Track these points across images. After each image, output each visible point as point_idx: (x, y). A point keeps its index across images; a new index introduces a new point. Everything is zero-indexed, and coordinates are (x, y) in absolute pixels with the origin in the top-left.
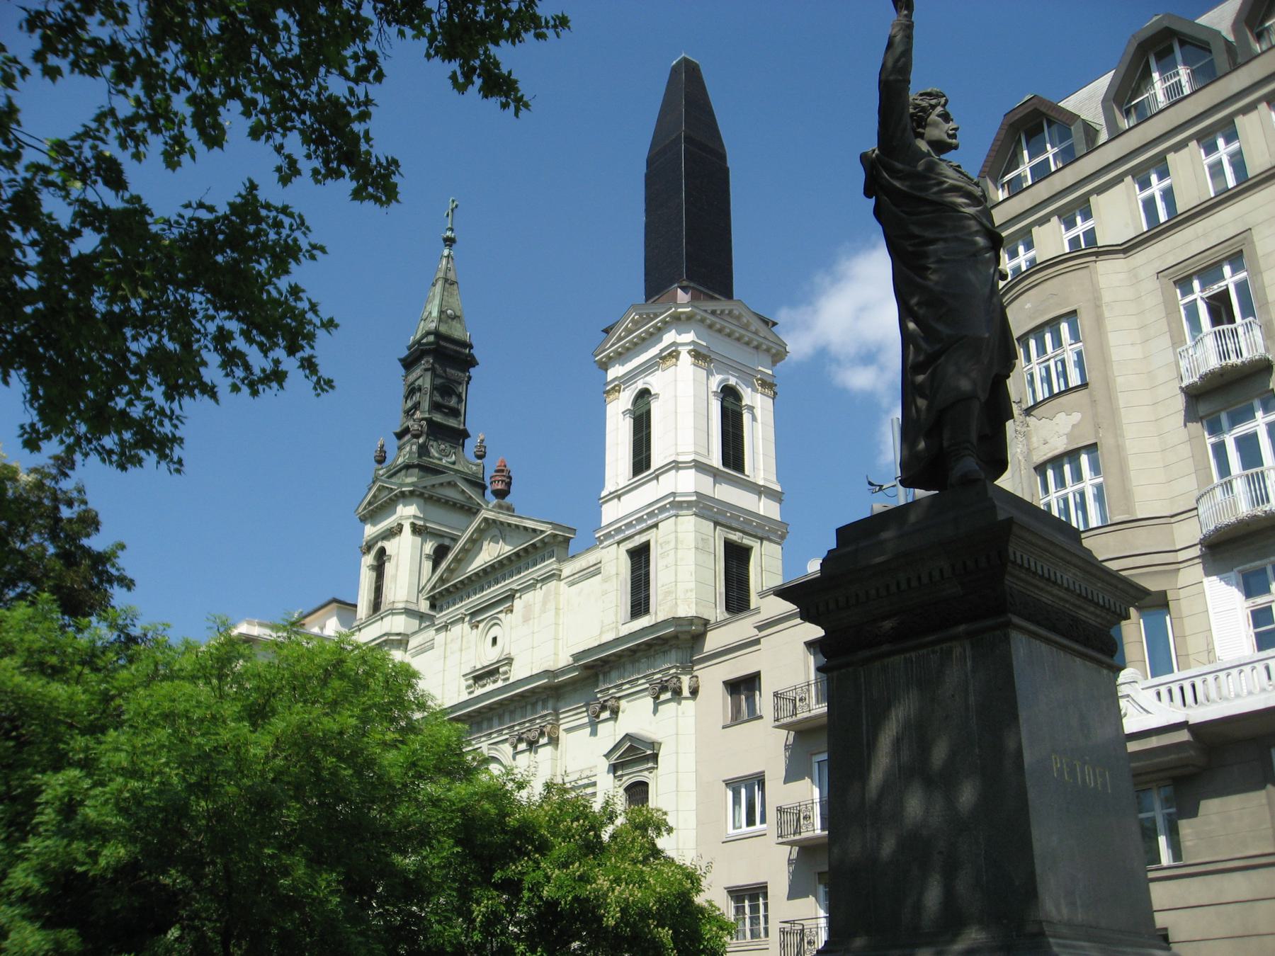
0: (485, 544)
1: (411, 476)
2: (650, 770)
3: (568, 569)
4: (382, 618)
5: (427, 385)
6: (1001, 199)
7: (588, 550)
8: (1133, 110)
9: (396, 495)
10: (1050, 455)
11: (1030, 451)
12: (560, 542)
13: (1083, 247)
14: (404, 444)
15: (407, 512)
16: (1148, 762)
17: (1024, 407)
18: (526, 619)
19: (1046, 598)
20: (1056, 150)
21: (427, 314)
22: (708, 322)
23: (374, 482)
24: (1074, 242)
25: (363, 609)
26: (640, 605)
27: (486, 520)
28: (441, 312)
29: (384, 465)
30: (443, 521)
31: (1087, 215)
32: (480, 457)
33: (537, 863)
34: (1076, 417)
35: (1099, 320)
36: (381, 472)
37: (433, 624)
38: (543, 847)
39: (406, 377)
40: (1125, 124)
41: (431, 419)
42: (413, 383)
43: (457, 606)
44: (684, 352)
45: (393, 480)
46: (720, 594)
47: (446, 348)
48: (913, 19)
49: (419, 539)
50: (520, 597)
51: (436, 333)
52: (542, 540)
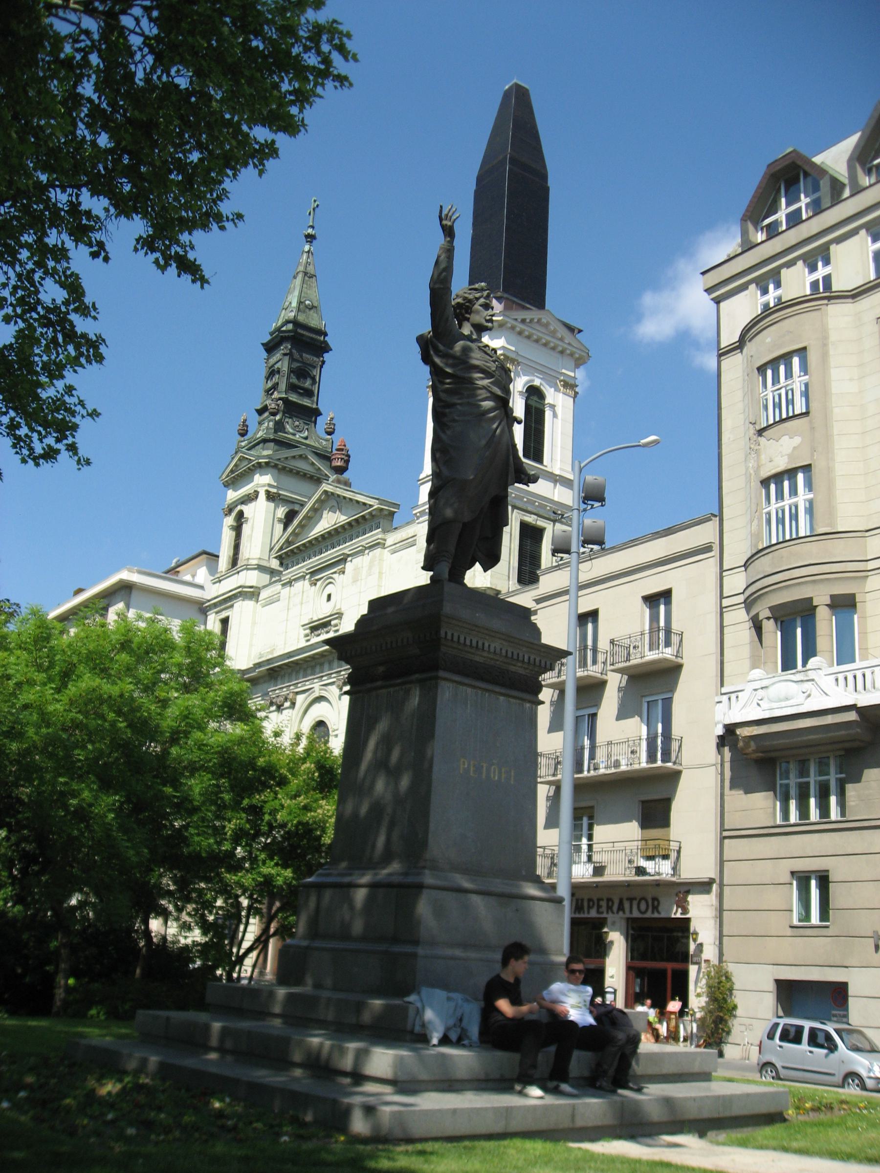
0: (325, 512)
1: (267, 449)
3: (392, 538)
4: (238, 572)
6: (759, 241)
7: (408, 523)
8: (874, 170)
9: (253, 465)
10: (774, 472)
11: (759, 467)
12: (386, 515)
13: (821, 290)
14: (264, 420)
15: (263, 481)
16: (824, 735)
17: (758, 428)
18: (355, 580)
19: (477, 659)
20: (808, 200)
21: (287, 303)
22: (518, 329)
23: (236, 453)
24: (815, 285)
25: (223, 563)
27: (326, 492)
28: (300, 303)
29: (246, 437)
30: (293, 489)
31: (827, 262)
32: (330, 433)
33: (276, 793)
34: (797, 440)
36: (243, 444)
37: (280, 580)
38: (283, 782)
39: (268, 359)
40: (865, 181)
41: (287, 398)
42: (273, 366)
43: (300, 565)
45: (251, 452)
46: (513, 568)
47: (303, 335)
48: (454, 244)
49: (272, 505)
50: (351, 561)
51: (295, 322)
52: (370, 513)
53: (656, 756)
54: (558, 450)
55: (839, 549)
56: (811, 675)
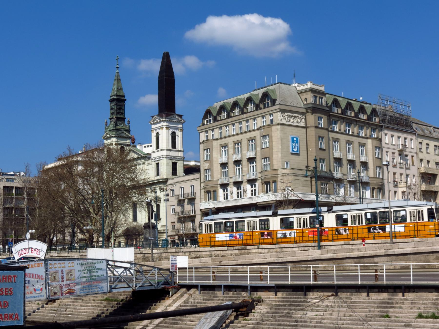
2: (160, 203)
3: (146, 162)
5: (116, 108)
26: (158, 174)
28: (117, 89)
32: (129, 124)
35: (212, 150)
44: (164, 127)
53: (377, 220)
54: (179, 145)
55: (273, 173)
56: (269, 195)
